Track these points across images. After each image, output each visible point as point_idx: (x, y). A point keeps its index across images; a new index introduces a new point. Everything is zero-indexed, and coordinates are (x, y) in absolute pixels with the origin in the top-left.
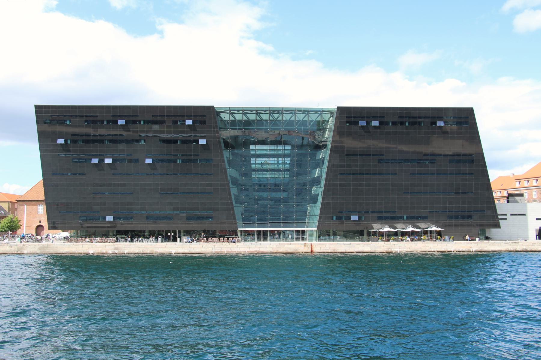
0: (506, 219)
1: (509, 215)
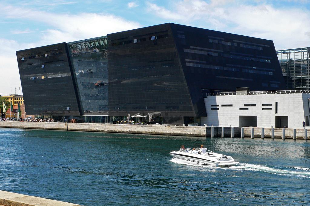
0: (271, 109)
1: (220, 106)
